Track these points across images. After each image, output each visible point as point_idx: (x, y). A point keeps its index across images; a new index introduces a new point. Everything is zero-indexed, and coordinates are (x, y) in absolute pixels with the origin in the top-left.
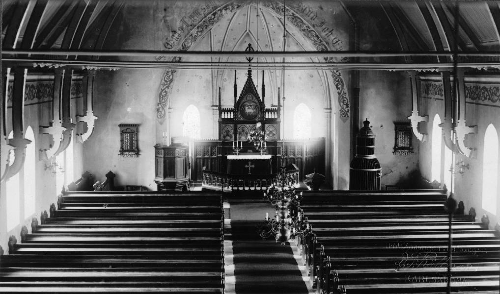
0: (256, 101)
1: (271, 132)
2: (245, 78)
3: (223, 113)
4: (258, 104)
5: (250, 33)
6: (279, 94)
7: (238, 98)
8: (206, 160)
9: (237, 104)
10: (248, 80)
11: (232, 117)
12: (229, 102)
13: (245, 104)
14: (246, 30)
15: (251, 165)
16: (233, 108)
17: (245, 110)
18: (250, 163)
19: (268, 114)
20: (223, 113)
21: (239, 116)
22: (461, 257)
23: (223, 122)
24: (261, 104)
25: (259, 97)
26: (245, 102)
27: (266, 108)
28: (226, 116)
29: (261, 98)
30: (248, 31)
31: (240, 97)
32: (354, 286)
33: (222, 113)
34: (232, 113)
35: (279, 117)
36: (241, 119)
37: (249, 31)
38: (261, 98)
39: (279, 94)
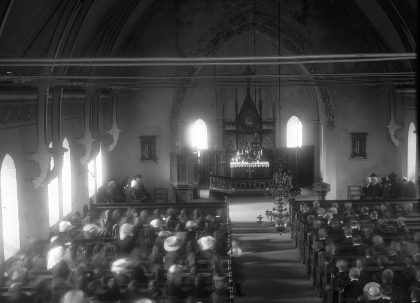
1: (268, 141)
7: (239, 112)
17: (245, 122)
24: (260, 118)
26: (245, 116)
31: (240, 112)
38: (259, 112)
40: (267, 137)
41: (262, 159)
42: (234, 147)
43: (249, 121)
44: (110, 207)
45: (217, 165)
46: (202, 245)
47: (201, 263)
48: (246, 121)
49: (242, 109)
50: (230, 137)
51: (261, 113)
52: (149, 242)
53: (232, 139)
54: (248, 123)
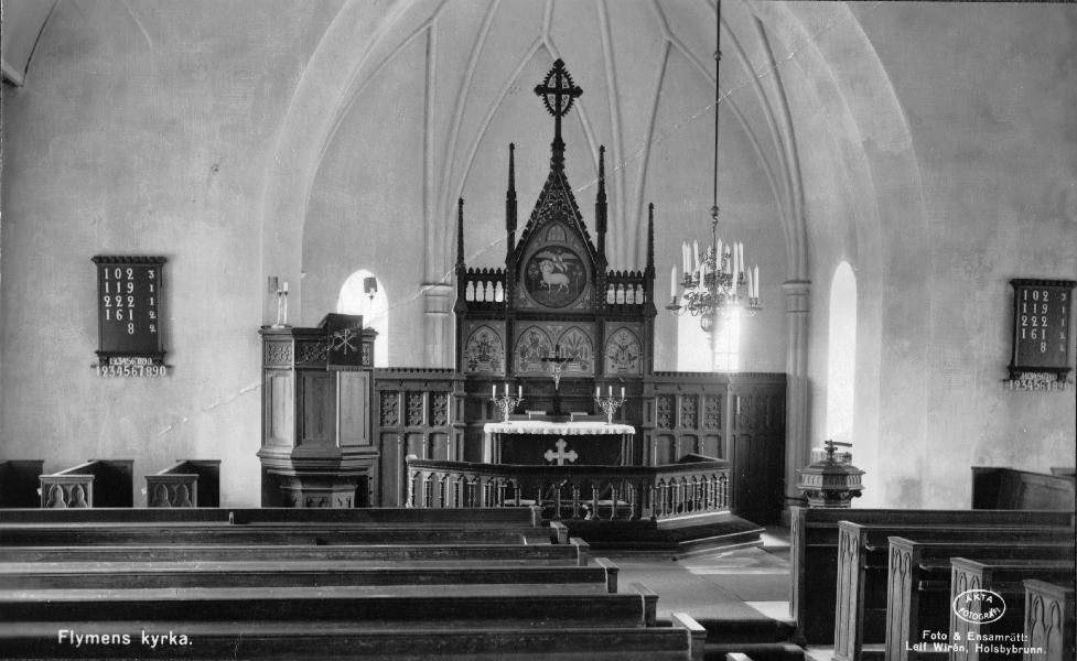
0: (577, 247)
1: (623, 349)
2: (545, 171)
3: (470, 283)
4: (584, 257)
5: (549, 47)
6: (461, 235)
7: (518, 236)
8: (900, 549)
9: (515, 255)
10: (551, 177)
11: (500, 298)
12: (490, 246)
13: (540, 255)
14: (539, 37)
15: (567, 450)
16: (503, 267)
17: (540, 276)
18: (561, 444)
19: (475, 286)
20: (470, 283)
21: (522, 296)
22: (997, 643)
23: (471, 314)
24: (598, 257)
25: (588, 236)
26: (538, 253)
27: (608, 270)
28: (476, 293)
29: (594, 238)
30: (545, 40)
31: (525, 233)
32: (332, 588)
33: (466, 285)
34: (499, 284)
35: (651, 297)
36: (530, 305)
37: (550, 39)
38: (594, 238)
39: (461, 235)
40: (624, 332)
41: (617, 419)
42: (495, 365)
43: (556, 271)
44: (340, 474)
45: (432, 436)
46: (826, 393)
47: (671, 527)
48: (546, 268)
49: (529, 224)
50: (484, 330)
51: (601, 240)
52: (798, 374)
53: (491, 337)
54: (553, 275)
